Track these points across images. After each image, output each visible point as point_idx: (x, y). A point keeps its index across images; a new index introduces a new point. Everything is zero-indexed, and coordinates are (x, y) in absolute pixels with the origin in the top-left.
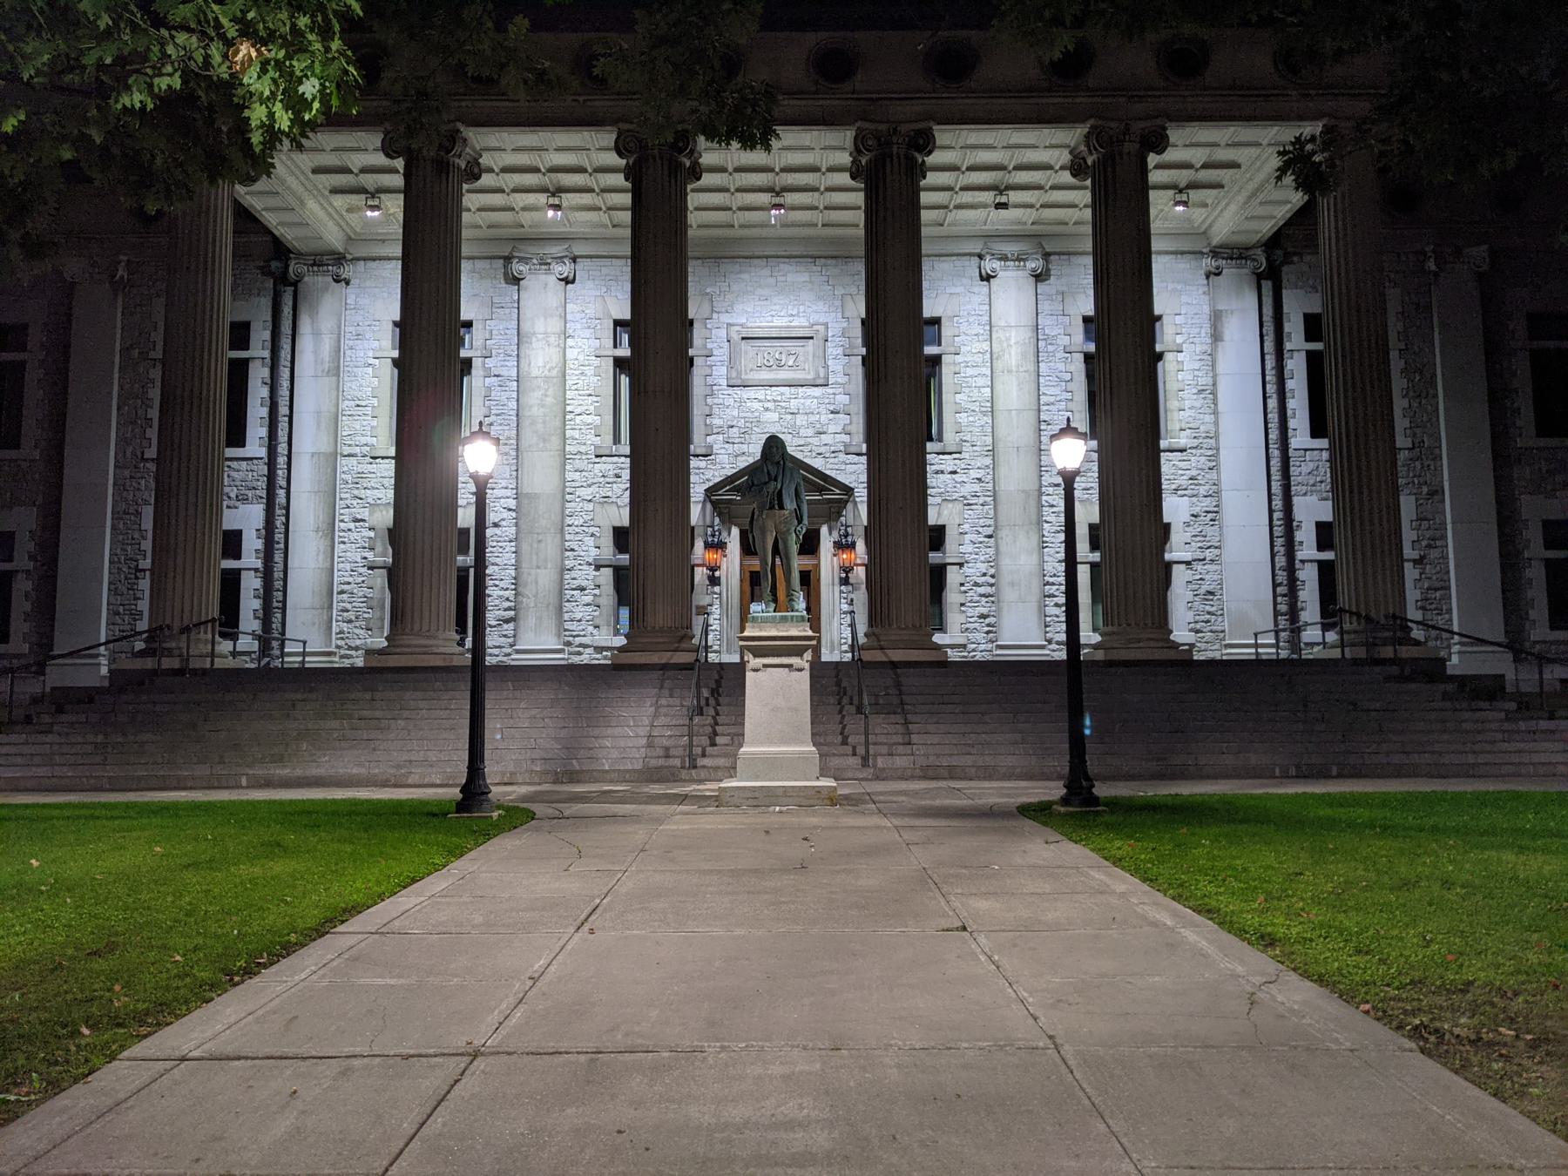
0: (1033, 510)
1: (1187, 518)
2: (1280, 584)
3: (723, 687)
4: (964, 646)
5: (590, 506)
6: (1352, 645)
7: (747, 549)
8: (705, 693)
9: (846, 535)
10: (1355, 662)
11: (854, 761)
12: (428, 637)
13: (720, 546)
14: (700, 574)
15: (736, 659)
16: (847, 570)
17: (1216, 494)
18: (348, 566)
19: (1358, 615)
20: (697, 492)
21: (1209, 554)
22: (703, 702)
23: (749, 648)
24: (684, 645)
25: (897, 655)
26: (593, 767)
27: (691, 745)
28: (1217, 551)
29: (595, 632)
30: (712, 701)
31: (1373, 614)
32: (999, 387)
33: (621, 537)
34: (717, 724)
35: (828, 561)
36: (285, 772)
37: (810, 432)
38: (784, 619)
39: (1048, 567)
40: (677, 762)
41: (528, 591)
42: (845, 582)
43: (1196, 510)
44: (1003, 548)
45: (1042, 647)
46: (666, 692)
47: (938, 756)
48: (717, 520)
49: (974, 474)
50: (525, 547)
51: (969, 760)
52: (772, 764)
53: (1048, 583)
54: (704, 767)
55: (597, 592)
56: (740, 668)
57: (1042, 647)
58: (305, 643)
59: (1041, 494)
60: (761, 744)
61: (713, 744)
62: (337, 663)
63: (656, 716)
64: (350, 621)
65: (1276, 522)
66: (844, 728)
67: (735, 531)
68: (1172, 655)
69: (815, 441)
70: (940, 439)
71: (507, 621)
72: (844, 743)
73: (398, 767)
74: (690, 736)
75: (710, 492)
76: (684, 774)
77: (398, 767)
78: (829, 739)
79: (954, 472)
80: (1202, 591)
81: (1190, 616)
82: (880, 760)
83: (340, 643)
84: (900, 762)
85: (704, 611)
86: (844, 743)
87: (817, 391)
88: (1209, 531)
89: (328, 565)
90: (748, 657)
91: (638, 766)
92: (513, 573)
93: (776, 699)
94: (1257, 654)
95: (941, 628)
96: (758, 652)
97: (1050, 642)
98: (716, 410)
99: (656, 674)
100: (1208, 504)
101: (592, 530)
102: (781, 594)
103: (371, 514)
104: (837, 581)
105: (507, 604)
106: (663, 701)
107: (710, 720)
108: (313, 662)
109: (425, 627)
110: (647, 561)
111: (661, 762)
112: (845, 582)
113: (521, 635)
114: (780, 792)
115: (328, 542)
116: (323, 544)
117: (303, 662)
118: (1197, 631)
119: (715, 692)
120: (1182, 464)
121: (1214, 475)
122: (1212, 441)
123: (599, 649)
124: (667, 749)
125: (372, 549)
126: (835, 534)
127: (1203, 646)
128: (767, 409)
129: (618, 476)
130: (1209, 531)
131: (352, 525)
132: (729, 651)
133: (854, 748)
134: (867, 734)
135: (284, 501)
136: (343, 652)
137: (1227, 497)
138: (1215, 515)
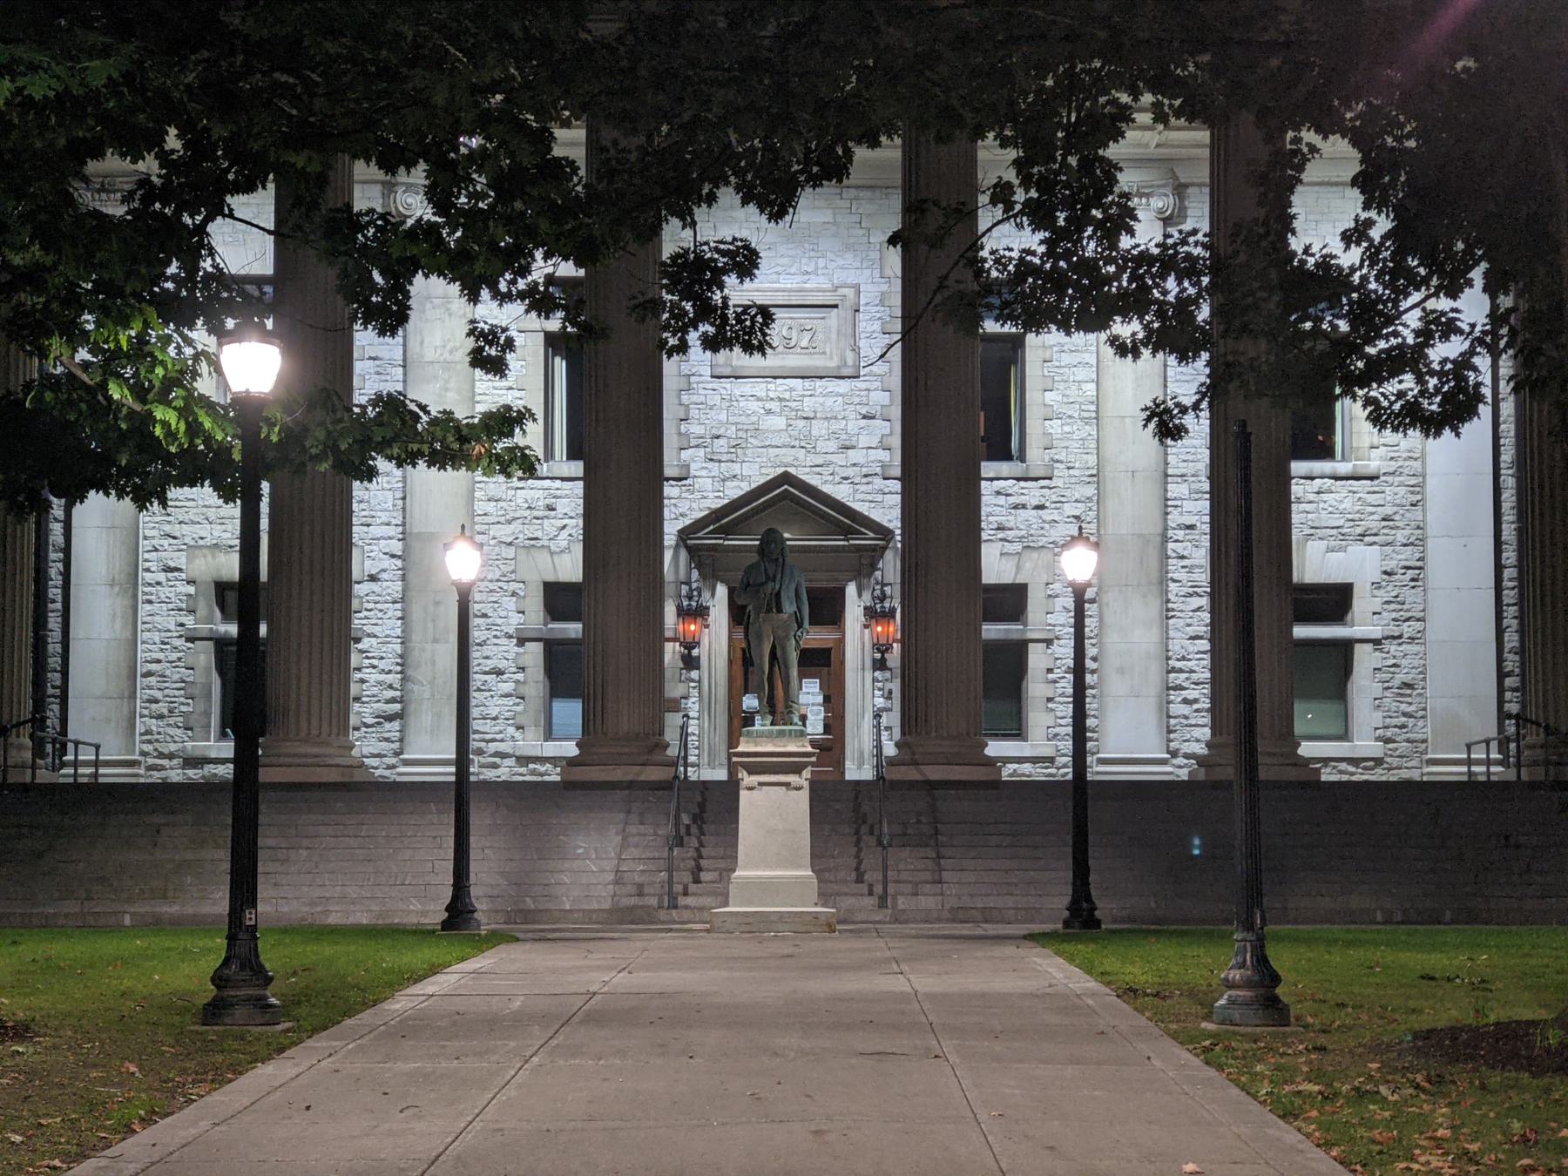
0: (1154, 563)
1: (1377, 577)
2: (1509, 674)
3: (709, 813)
4: (1051, 760)
5: (511, 552)
6: (1535, 763)
7: (737, 615)
8: (686, 819)
9: (883, 598)
10: (1532, 785)
11: (870, 902)
12: (318, 744)
13: (700, 613)
14: (671, 651)
15: (721, 775)
16: (882, 648)
17: (1419, 543)
18: (157, 637)
19: (1538, 725)
20: (671, 530)
21: (1408, 629)
22: (683, 831)
23: (743, 765)
24: (657, 758)
25: (935, 773)
26: (551, 906)
27: (670, 882)
28: (1419, 625)
29: (518, 735)
30: (694, 830)
31: (1552, 722)
32: (1108, 383)
33: (559, 599)
34: (700, 857)
35: (856, 635)
36: (173, 909)
37: (832, 446)
38: (781, 734)
39: (1178, 645)
40: (654, 901)
41: (420, 674)
42: (880, 665)
43: (1390, 565)
44: (1108, 619)
45: (1163, 762)
46: (634, 817)
47: (972, 896)
48: (695, 574)
49: (1070, 510)
50: (416, 612)
51: (1010, 902)
52: (766, 889)
53: (1174, 670)
54: (686, 907)
55: (520, 676)
56: (731, 789)
57: (1163, 762)
58: (98, 747)
59: (1165, 539)
60: (757, 866)
61: (697, 881)
62: (142, 776)
63: (624, 846)
64: (161, 717)
65: (1506, 584)
66: (860, 863)
67: (722, 590)
68: (1291, 774)
69: (839, 459)
70: (1022, 459)
71: (390, 718)
72: (860, 880)
73: (312, 904)
74: (670, 870)
75: (684, 534)
76: (663, 915)
77: (312, 904)
78: (841, 875)
79: (1041, 507)
80: (1396, 682)
81: (1377, 718)
82: (901, 900)
83: (147, 748)
84: (927, 902)
85: (675, 706)
86: (860, 880)
87: (843, 386)
88: (1409, 595)
89: (128, 634)
90: (742, 774)
91: (607, 905)
92: (398, 649)
93: (773, 817)
94: (1470, 773)
95: (1017, 731)
96: (753, 769)
97: (1174, 754)
98: (694, 413)
99: (620, 794)
100: (1408, 556)
101: (514, 586)
102: (780, 706)
103: (189, 561)
104: (868, 663)
105: (390, 694)
106: (632, 829)
107: (692, 853)
108: (109, 775)
109: (314, 732)
110: (597, 638)
111: (634, 901)
112: (880, 665)
113: (410, 737)
114: (773, 918)
115: (128, 602)
116: (122, 603)
117: (96, 775)
118: (1387, 741)
119: (698, 818)
120: (1371, 498)
121: (1417, 514)
122: (1417, 464)
123: (523, 760)
124: (640, 886)
125: (192, 611)
126: (867, 596)
127: (1395, 762)
128: (769, 412)
129: (551, 508)
130: (1409, 595)
131: (162, 577)
132: (711, 765)
133: (871, 886)
134: (885, 869)
135: (60, 540)
136: (151, 761)
137: (1437, 549)
138: (1417, 572)
